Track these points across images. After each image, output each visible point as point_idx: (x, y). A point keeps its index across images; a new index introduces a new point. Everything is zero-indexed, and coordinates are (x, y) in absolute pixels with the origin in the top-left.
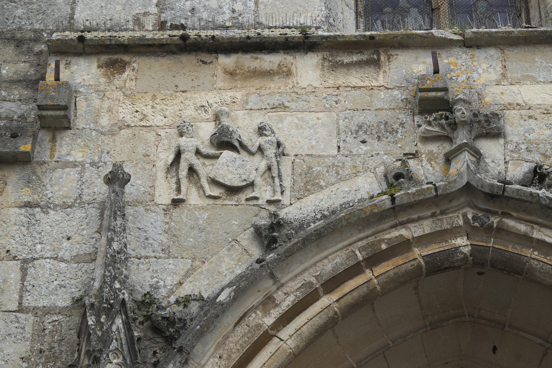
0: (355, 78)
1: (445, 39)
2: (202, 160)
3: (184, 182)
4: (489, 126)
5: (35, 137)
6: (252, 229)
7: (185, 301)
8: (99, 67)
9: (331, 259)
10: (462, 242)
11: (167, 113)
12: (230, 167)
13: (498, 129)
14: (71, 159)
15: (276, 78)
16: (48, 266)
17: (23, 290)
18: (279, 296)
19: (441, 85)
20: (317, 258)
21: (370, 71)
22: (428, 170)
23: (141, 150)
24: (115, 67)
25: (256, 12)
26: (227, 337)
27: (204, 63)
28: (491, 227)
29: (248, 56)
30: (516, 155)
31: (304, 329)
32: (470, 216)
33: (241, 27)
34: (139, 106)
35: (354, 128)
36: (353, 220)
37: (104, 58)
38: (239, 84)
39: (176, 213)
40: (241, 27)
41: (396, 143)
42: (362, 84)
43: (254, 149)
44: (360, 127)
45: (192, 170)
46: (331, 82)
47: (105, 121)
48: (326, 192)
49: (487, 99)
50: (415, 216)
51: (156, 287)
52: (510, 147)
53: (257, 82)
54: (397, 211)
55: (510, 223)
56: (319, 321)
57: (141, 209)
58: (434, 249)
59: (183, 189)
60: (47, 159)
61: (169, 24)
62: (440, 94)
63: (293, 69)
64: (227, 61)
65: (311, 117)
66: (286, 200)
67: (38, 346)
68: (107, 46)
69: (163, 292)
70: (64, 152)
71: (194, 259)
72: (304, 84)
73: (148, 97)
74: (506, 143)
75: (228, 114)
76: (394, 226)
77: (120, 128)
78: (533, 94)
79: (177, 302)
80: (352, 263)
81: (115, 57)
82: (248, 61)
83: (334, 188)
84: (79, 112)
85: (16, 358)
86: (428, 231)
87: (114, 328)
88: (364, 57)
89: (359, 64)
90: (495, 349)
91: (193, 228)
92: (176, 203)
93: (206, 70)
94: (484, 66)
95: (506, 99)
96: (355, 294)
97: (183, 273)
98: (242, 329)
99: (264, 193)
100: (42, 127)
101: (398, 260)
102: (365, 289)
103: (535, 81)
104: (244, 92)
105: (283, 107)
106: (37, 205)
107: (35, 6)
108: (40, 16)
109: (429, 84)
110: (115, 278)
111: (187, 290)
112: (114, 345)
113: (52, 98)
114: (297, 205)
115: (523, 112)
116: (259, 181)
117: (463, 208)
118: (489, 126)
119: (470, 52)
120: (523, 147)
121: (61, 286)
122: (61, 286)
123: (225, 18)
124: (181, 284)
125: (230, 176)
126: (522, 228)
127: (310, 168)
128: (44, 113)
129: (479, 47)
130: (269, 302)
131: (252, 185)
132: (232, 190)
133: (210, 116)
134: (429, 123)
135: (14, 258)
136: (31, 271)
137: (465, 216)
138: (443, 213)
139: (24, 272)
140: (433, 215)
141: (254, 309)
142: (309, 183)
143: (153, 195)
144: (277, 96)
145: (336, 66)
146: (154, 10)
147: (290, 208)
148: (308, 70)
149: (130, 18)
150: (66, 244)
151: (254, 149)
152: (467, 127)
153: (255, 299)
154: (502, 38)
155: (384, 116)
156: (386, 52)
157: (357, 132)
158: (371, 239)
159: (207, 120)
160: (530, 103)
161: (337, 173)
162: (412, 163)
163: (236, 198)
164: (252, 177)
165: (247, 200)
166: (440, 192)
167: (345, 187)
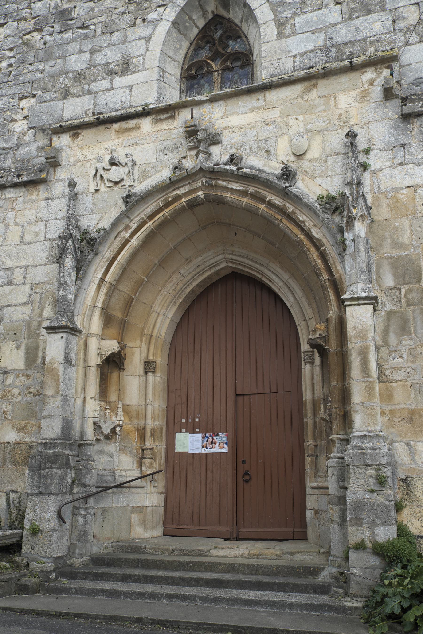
0: (164, 126)
1: (200, 100)
2: (106, 172)
3: (99, 182)
4: (214, 140)
5: (48, 171)
6: (122, 200)
7: (98, 231)
8: (70, 137)
9: (150, 207)
10: (200, 194)
11: (94, 153)
12: (115, 173)
13: (217, 140)
14: (61, 178)
15: (134, 131)
16: (54, 222)
17: (46, 233)
18: (131, 225)
19: (193, 124)
20: (144, 208)
21: (171, 121)
22: (189, 164)
23: (84, 171)
24: (75, 136)
25: (130, 100)
26: (112, 243)
27: (108, 128)
28: (212, 185)
29: (124, 122)
30: (225, 151)
31: (140, 237)
32: (204, 182)
33: (124, 109)
34: (84, 152)
35: (163, 149)
36: (155, 190)
37: (72, 133)
38: (120, 136)
39: (96, 195)
40: (124, 109)
41: (178, 153)
42: (167, 128)
43: (124, 164)
44: (165, 148)
45: (102, 177)
46: (155, 129)
47: (72, 160)
48: (151, 179)
49: (216, 127)
50: (182, 185)
51: (89, 226)
52: (223, 147)
53: (127, 134)
54: (173, 183)
55: (220, 182)
56: (146, 233)
57: (84, 195)
58: (190, 197)
59: (98, 185)
60: (52, 179)
61: (96, 113)
62: (193, 128)
63: (141, 126)
64: (116, 126)
65: (146, 146)
66: (135, 184)
67: (51, 253)
68: (72, 127)
69: (92, 228)
70: (58, 176)
71: (102, 213)
72: (144, 132)
73: (87, 147)
74: (222, 146)
75: (115, 151)
76: (174, 190)
77: (77, 162)
78: (235, 120)
79: (96, 231)
80: (158, 208)
81: (75, 132)
82: (124, 125)
83: (153, 177)
84: (63, 158)
85: (44, 258)
86: (187, 190)
87: (68, 244)
88: (169, 115)
89: (167, 118)
90: (236, 234)
91: (102, 201)
92: (97, 191)
93: (108, 131)
94: (217, 110)
95: (224, 125)
96: (159, 220)
97: (98, 219)
98: (118, 239)
99: (128, 182)
100: (51, 166)
101: (176, 204)
102: (163, 218)
103: (237, 113)
104: (122, 139)
105: (136, 143)
106: (50, 199)
107: (49, 113)
108: (51, 117)
109: (188, 124)
110: (70, 225)
111: (100, 226)
112: (69, 250)
113: (49, 154)
114: (140, 186)
115: (231, 130)
116: (125, 178)
117: (201, 178)
118: (214, 140)
119: (212, 104)
120: (229, 146)
121: (58, 230)
122: (58, 230)
123: (118, 106)
124: (98, 224)
125: (114, 177)
126: (224, 184)
127: (145, 169)
128: (48, 161)
129: (216, 101)
130: (127, 227)
131: (123, 180)
132: (116, 183)
133: (109, 152)
134: (190, 142)
135: (43, 220)
136: (48, 225)
137: (202, 182)
138: (193, 182)
139: (46, 225)
140: (189, 183)
141: (122, 231)
142: (145, 176)
143: (88, 189)
144: (134, 139)
145: (158, 121)
146: (92, 107)
147: (137, 188)
148: (146, 124)
149: (84, 112)
150: (60, 213)
151: (124, 164)
152: (204, 142)
153: (122, 227)
154: (224, 95)
155: (175, 141)
156: (178, 111)
157: (164, 150)
158: (166, 197)
159: (108, 154)
160: (234, 125)
161: (155, 170)
162: (184, 161)
163: (117, 186)
164: (122, 177)
165: (121, 186)
166: (189, 173)
167: (157, 176)
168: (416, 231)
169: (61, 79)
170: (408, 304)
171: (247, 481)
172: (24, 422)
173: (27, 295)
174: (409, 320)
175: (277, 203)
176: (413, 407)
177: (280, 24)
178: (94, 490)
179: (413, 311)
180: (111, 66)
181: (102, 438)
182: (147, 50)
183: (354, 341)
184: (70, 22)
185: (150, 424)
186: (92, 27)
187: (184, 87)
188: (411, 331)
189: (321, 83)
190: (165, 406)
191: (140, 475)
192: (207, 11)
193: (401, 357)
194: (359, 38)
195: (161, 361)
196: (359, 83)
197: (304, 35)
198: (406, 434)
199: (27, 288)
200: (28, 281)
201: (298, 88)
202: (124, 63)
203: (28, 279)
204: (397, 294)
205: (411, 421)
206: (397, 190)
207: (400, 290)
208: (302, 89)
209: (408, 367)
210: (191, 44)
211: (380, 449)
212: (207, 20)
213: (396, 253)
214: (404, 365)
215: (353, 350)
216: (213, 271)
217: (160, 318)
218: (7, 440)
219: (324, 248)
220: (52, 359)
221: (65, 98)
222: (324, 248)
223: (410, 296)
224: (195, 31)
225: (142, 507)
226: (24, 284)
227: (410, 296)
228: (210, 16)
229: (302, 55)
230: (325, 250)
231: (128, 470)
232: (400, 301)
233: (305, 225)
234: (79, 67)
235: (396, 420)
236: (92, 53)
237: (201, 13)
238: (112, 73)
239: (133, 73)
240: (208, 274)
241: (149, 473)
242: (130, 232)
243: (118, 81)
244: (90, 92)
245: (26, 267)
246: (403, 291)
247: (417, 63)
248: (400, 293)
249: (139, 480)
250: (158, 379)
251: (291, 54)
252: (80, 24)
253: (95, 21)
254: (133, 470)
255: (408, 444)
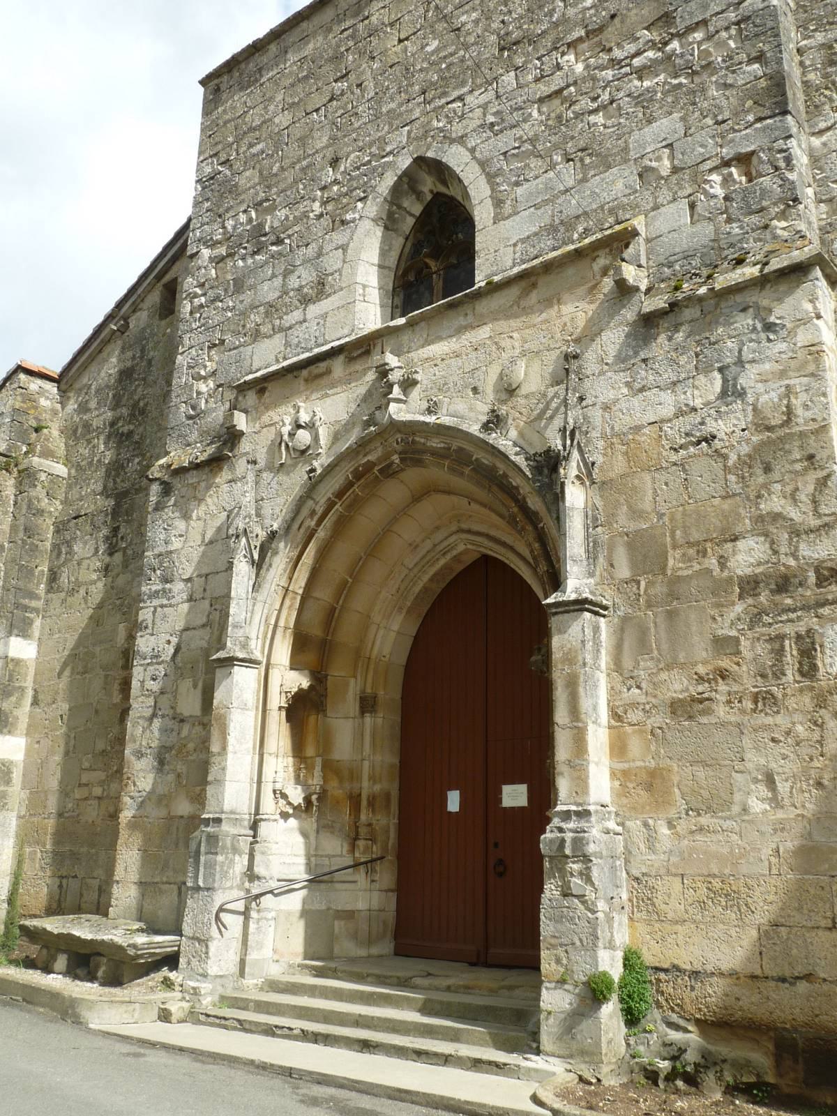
24: (262, 391)
64: (305, 373)
82: (315, 369)
89: (360, 356)
98: (302, 530)
146: (283, 349)
168: (662, 490)
169: (252, 316)
170: (649, 605)
171: (501, 875)
172: (199, 788)
173: (206, 613)
174: (649, 629)
175: (486, 462)
176: (653, 764)
177: (498, 203)
178: (273, 884)
179: (655, 615)
180: (305, 290)
181: (291, 811)
182: (344, 262)
183: (560, 666)
184: (263, 239)
185: (366, 787)
186: (287, 241)
187: (398, 301)
188: (651, 646)
189: (542, 281)
190: (396, 761)
191: (352, 863)
192: (422, 192)
193: (639, 687)
194: (594, 206)
195: (390, 693)
196: (590, 275)
197: (527, 213)
198: (643, 807)
199: (207, 602)
200: (208, 594)
201: (514, 291)
202: (319, 283)
203: (208, 592)
204: (634, 589)
205: (649, 787)
206: (637, 429)
207: (638, 583)
208: (518, 293)
209: (648, 703)
210: (407, 239)
211: (585, 832)
212: (426, 203)
213: (632, 526)
214: (643, 699)
215: (559, 681)
216: (448, 557)
217: (381, 632)
218: (180, 813)
219: (542, 525)
220: (221, 702)
221: (255, 340)
222: (542, 525)
223: (652, 591)
224: (410, 221)
225: (353, 912)
226: (203, 598)
227: (652, 591)
228: (429, 197)
229: (523, 241)
230: (543, 528)
231: (334, 856)
232: (638, 600)
233: (519, 494)
234: (272, 296)
235: (631, 785)
236: (285, 277)
237: (414, 197)
238: (306, 301)
239: (330, 295)
240: (442, 562)
241: (362, 860)
242: (316, 518)
243: (314, 310)
244: (281, 329)
245: (207, 575)
246: (643, 584)
247: (669, 232)
248: (639, 588)
249: (350, 870)
250: (380, 721)
251: (511, 243)
252: (273, 238)
253: (290, 232)
254: (341, 856)
255: (646, 825)
